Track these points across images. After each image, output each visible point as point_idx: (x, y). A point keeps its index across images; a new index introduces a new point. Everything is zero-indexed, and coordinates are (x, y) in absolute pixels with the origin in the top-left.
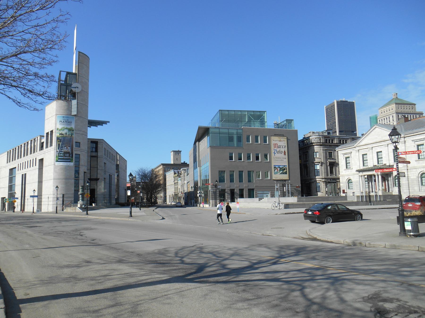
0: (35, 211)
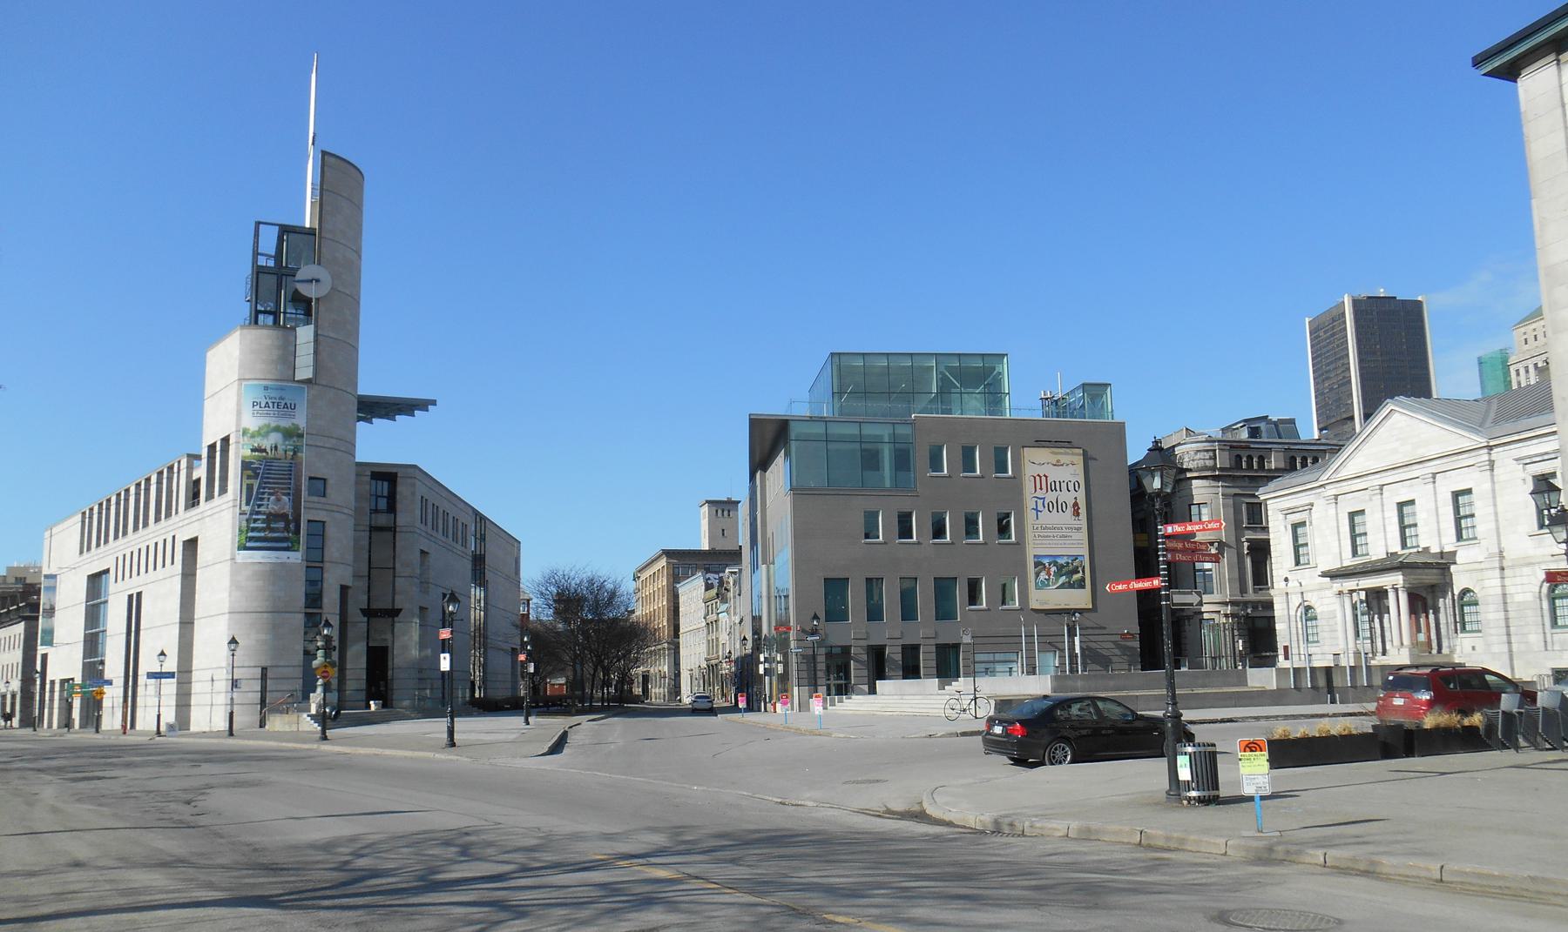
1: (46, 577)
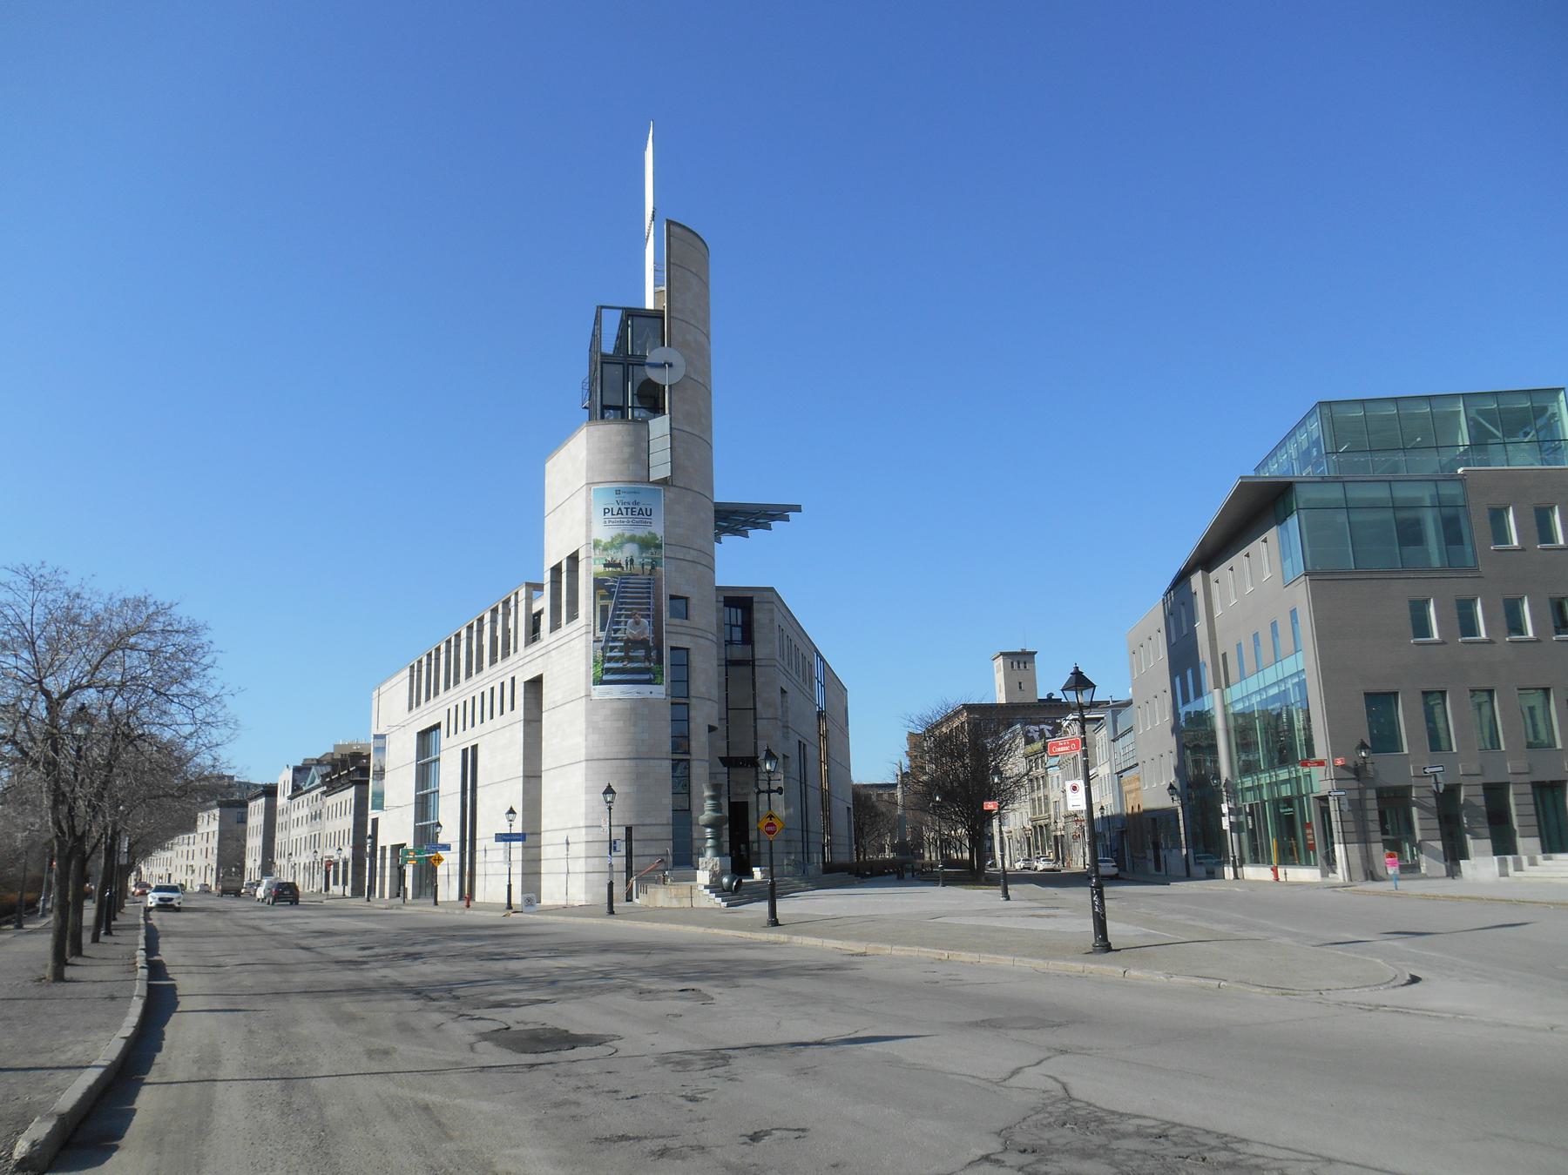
0: (517, 899)
1: (376, 737)
